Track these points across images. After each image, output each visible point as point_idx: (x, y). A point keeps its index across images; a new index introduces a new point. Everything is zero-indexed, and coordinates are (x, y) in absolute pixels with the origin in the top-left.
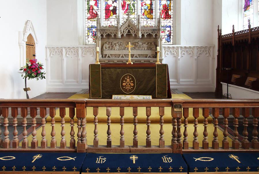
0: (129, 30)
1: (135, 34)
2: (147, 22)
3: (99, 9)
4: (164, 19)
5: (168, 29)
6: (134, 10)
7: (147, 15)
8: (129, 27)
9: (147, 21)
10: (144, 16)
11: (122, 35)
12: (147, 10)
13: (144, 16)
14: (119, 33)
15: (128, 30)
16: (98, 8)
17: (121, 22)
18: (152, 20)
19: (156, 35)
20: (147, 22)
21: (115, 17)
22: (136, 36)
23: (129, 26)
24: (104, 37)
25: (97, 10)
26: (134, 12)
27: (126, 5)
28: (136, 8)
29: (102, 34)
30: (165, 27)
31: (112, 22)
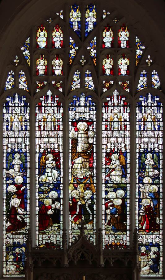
0: (82, 254)
1: (92, 260)
2: (116, 237)
3: (28, 213)
4: (147, 231)
5: (154, 249)
6: (91, 216)
7: (116, 225)
8: (82, 248)
9: (116, 236)
10: (110, 225)
11: (71, 263)
12: (116, 216)
13: (110, 225)
14: (66, 258)
15: (81, 253)
16: (27, 211)
17: (71, 239)
18: (125, 233)
19: (130, 262)
20: (116, 237)
21: (56, 228)
22: (96, 264)
23: (83, 246)
24: (40, 265)
25: (24, 215)
26: (91, 218)
27: (78, 207)
28: (95, 212)
29: (107, 260)
30: (148, 245)
31: (53, 236)
